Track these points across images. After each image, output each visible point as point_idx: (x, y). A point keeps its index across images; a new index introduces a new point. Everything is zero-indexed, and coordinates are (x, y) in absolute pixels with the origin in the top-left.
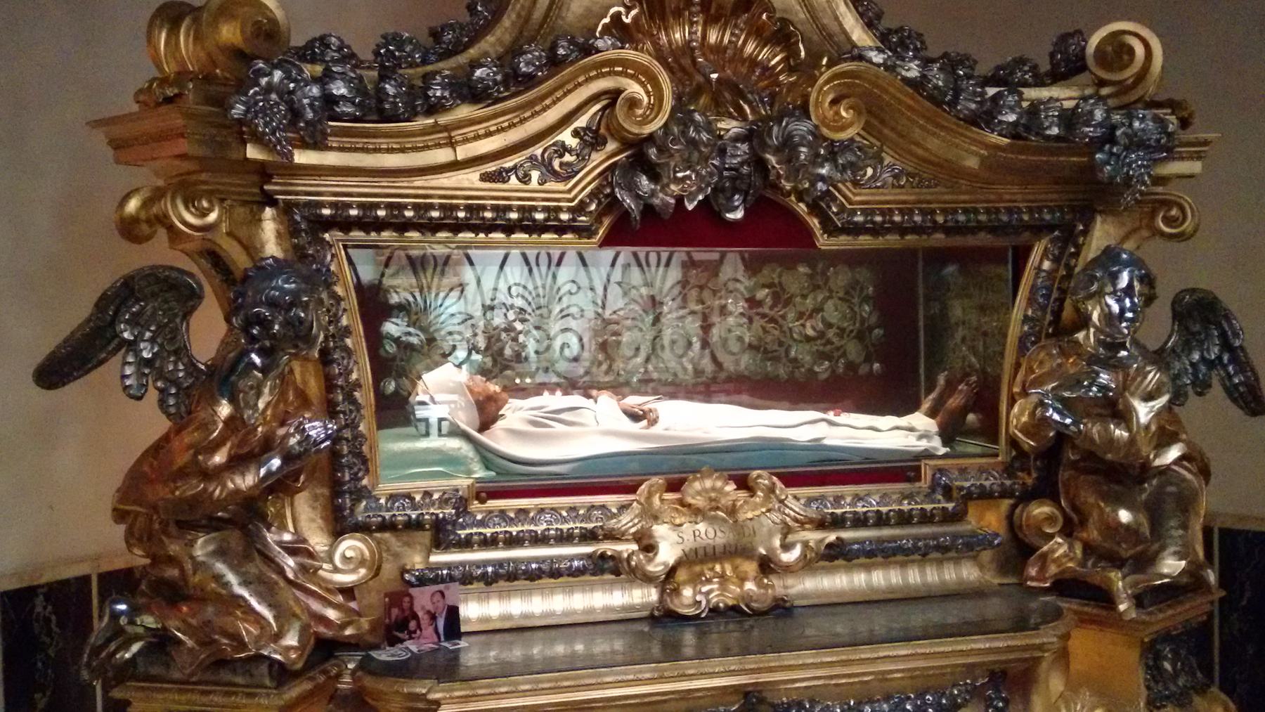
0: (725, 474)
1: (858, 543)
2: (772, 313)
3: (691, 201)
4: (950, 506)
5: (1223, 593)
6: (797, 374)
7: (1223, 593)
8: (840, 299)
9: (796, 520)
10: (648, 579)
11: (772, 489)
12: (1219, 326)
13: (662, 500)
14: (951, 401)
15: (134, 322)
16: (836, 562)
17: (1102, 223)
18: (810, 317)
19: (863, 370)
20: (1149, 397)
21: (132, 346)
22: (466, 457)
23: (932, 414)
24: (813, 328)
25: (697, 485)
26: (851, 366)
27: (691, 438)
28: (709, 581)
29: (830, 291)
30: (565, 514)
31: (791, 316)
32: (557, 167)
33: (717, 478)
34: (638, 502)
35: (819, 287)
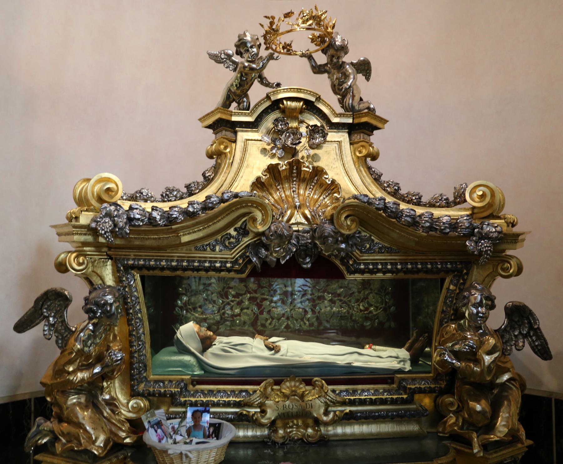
0: (301, 378)
1: (360, 413)
2: (345, 299)
3: (283, 259)
4: (405, 396)
5: (530, 442)
6: (356, 326)
7: (530, 442)
8: (376, 293)
9: (331, 401)
10: (262, 426)
11: (322, 387)
12: (528, 318)
13: (272, 390)
14: (416, 345)
15: (48, 309)
16: (351, 421)
17: (477, 269)
18: (362, 301)
19: (387, 325)
20: (489, 353)
21: (47, 318)
22: (192, 365)
23: (408, 350)
24: (363, 306)
25: (288, 384)
26: (381, 323)
27: (293, 361)
28: (291, 427)
29: (371, 290)
30: (229, 393)
31: (353, 301)
32: (227, 244)
33: (297, 381)
34: (260, 391)
35: (366, 288)
